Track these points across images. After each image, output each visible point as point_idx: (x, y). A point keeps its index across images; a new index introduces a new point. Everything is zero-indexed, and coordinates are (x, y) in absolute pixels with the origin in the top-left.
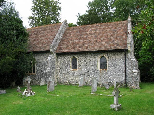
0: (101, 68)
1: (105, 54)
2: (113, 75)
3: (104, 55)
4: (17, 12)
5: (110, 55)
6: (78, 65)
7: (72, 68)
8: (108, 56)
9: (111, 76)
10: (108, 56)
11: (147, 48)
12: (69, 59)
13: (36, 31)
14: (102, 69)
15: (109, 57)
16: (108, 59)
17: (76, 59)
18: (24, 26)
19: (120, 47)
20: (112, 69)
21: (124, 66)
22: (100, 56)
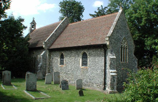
0: (82, 65)
1: (86, 50)
2: (93, 74)
3: (85, 51)
4: (33, 24)
5: (91, 51)
6: (64, 61)
7: (82, 65)
8: (89, 52)
9: (91, 75)
10: (89, 52)
11: (146, 42)
12: (59, 54)
13: (39, 36)
14: (83, 67)
15: (89, 54)
16: (89, 55)
17: (86, 55)
18: (96, 1)
19: (99, 42)
20: (92, 67)
21: (103, 64)
22: (82, 52)
